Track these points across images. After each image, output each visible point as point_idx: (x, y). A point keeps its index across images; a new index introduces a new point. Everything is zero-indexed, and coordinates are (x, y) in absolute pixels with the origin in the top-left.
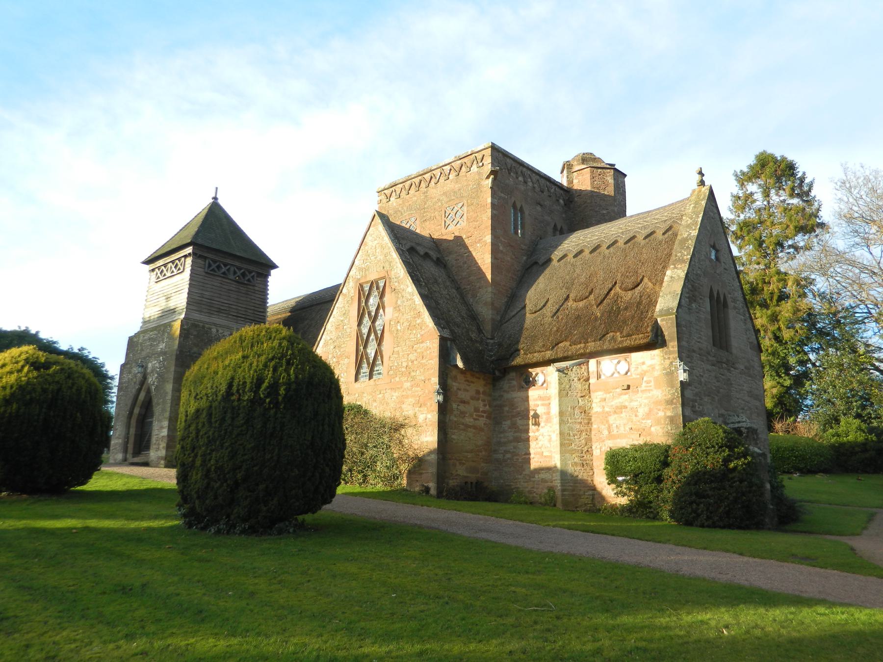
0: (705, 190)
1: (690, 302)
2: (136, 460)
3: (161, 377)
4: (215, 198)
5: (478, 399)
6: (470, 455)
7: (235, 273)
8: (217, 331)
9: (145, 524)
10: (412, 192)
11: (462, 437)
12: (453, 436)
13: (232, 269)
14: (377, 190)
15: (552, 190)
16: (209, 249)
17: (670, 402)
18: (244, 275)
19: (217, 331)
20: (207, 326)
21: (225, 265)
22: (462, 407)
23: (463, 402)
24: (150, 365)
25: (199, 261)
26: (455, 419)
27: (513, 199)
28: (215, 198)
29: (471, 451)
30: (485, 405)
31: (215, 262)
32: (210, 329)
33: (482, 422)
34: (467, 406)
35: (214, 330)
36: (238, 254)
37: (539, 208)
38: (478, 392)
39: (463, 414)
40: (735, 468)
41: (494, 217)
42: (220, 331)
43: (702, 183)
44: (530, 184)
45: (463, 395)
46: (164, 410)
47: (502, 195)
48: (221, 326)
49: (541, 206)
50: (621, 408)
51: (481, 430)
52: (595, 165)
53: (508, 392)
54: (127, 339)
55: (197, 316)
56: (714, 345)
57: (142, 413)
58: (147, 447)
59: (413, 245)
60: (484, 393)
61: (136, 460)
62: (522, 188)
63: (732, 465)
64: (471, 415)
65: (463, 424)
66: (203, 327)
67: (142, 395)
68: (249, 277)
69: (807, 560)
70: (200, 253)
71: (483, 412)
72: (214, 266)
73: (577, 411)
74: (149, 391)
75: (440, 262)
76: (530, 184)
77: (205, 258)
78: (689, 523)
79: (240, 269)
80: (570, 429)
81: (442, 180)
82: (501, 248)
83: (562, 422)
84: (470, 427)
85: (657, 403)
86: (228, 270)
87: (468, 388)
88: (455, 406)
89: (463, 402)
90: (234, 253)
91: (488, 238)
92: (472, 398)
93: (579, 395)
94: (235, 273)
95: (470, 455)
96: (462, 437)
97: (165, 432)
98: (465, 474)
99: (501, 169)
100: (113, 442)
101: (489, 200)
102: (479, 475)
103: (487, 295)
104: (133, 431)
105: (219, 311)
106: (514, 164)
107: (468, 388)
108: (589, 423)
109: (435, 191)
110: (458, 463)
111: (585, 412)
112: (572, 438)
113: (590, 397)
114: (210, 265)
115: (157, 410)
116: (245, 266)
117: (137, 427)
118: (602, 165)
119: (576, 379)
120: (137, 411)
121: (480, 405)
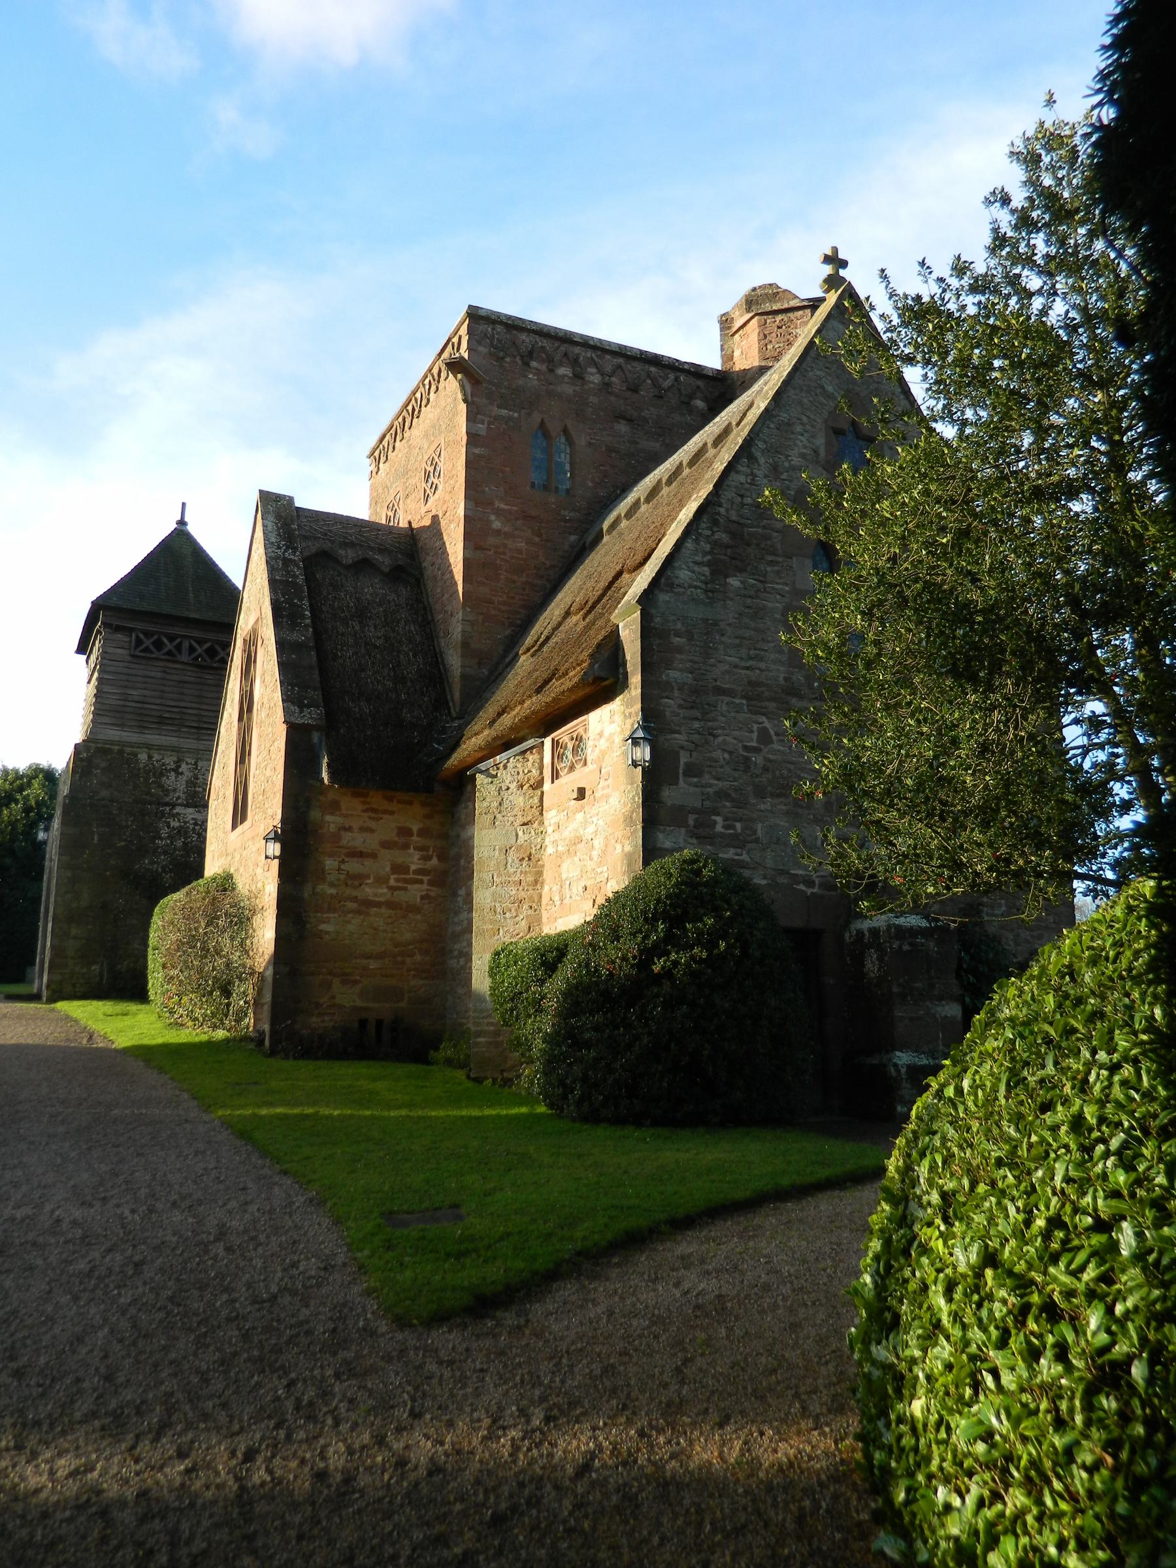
1: (719, 570)
4: (182, 522)
5: (406, 847)
6: (373, 965)
7: (192, 650)
8: (150, 757)
9: (488, 1112)
11: (350, 927)
12: (323, 927)
13: (186, 645)
14: (368, 453)
16: (135, 614)
19: (150, 757)
20: (128, 750)
21: (172, 639)
25: (119, 636)
26: (333, 891)
27: (537, 417)
28: (182, 522)
29: (380, 956)
30: (426, 858)
31: (148, 634)
32: (136, 755)
34: (368, 862)
35: (143, 757)
36: (193, 615)
37: (622, 427)
38: (405, 832)
39: (358, 879)
40: (667, 973)
42: (156, 757)
47: (504, 412)
48: (160, 748)
49: (630, 420)
51: (412, 909)
52: (768, 307)
59: (327, 546)
60: (422, 833)
63: (656, 968)
64: (381, 880)
65: (354, 899)
66: (121, 752)
70: (115, 622)
72: (148, 643)
73: (513, 856)
77: (131, 630)
78: (592, 1118)
79: (200, 642)
82: (497, 525)
84: (378, 905)
86: (179, 647)
87: (373, 825)
88: (330, 863)
90: (186, 614)
92: (386, 845)
93: (520, 820)
94: (192, 650)
95: (373, 965)
96: (350, 927)
98: (359, 1003)
103: (455, 628)
105: (161, 721)
107: (373, 825)
108: (537, 881)
110: (336, 982)
111: (530, 858)
113: (542, 823)
114: (139, 642)
116: (212, 636)
119: (513, 786)
121: (414, 861)
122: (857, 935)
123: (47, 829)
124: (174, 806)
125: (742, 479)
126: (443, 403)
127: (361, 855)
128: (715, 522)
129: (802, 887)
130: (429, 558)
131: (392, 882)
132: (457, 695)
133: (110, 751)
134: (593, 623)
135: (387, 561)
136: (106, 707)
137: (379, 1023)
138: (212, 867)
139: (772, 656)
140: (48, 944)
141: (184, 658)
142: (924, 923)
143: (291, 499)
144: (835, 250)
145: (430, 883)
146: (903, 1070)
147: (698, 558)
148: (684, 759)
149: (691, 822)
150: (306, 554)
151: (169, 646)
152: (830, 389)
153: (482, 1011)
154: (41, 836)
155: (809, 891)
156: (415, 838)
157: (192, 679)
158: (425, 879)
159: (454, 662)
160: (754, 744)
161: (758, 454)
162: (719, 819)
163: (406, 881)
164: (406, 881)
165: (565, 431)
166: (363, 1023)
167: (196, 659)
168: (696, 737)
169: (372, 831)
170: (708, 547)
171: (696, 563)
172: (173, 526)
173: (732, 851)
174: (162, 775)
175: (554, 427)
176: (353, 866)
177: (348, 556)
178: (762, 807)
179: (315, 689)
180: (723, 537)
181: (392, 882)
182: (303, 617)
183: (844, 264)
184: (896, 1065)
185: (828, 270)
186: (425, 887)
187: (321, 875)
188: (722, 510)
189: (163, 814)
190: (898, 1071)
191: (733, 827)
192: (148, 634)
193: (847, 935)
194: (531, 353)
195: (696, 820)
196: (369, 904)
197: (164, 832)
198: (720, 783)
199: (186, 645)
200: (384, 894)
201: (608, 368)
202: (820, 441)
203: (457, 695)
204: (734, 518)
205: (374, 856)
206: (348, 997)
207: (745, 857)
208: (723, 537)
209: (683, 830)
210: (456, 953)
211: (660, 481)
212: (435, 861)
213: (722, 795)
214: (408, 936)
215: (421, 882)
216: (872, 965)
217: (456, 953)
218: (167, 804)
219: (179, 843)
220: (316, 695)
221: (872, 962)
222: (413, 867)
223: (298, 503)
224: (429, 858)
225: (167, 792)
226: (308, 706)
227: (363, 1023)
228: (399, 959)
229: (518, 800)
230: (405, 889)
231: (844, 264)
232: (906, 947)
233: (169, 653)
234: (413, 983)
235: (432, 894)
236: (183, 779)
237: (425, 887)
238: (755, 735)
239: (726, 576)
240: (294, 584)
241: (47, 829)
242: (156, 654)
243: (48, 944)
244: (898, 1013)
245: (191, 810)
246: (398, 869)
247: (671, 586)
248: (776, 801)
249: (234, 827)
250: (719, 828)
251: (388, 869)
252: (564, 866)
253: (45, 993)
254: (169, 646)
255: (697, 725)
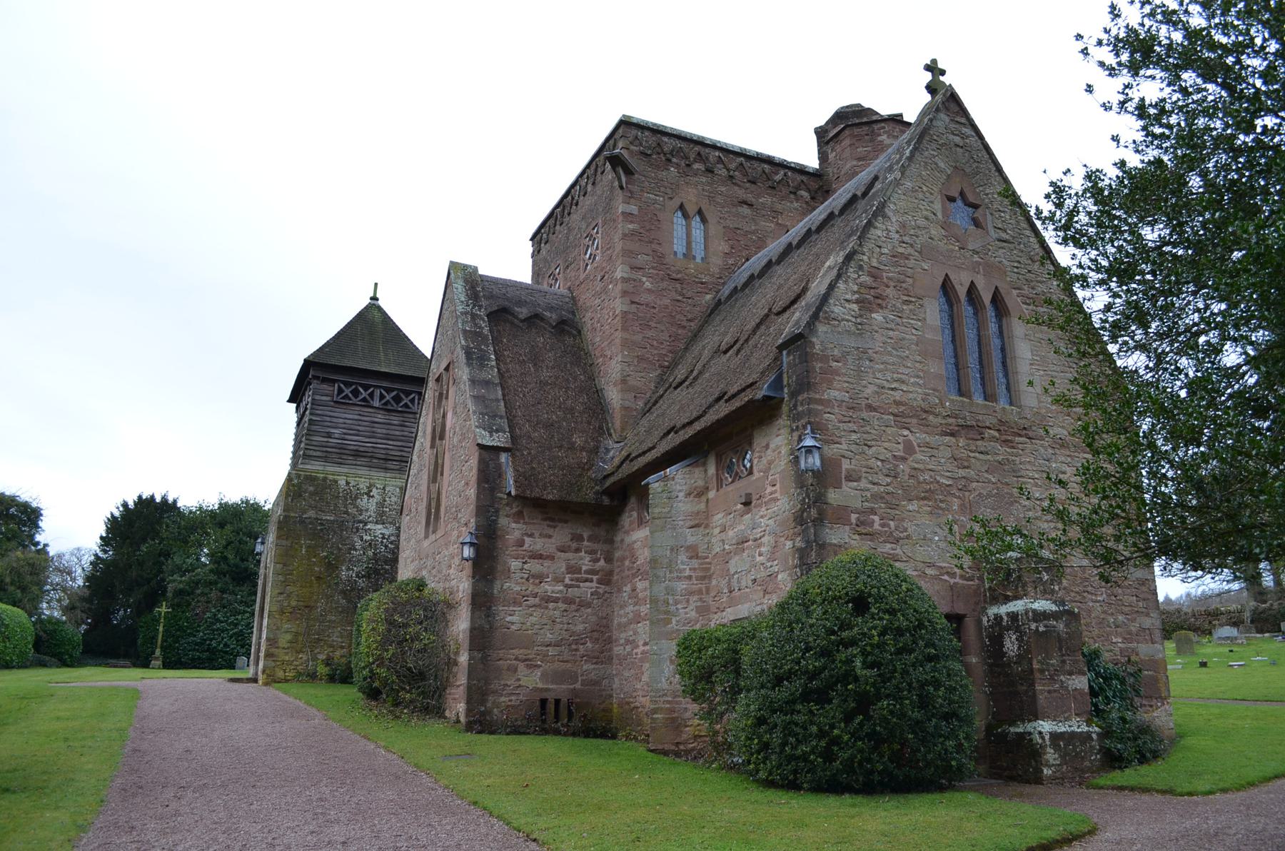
4: (374, 298)
5: (578, 550)
8: (348, 483)
13: (377, 393)
20: (331, 477)
21: (366, 388)
28: (374, 298)
35: (342, 483)
51: (583, 604)
53: (627, 532)
54: (26, 494)
64: (558, 580)
66: (325, 479)
68: (406, 401)
72: (347, 391)
75: (959, 390)
77: (334, 381)
79: (389, 390)
84: (556, 600)
86: (371, 395)
88: (515, 564)
90: (378, 369)
94: (382, 397)
98: (540, 685)
102: (578, 686)
106: (679, 144)
107: (550, 531)
110: (521, 666)
112: (673, 608)
114: (340, 391)
121: (585, 562)
122: (995, 619)
123: (263, 543)
124: (366, 524)
125: (879, 233)
126: (599, 192)
127: (541, 557)
128: (861, 268)
129: (946, 577)
130: (589, 315)
131: (567, 581)
132: (618, 424)
133: (316, 478)
134: (747, 358)
135: (554, 316)
136: (305, 446)
137: (557, 702)
138: (405, 572)
139: (912, 380)
140: (264, 636)
141: (376, 403)
142: (1054, 608)
143: (476, 269)
144: (934, 61)
145: (599, 582)
146: (1047, 737)
147: (848, 297)
148: (846, 465)
149: (854, 521)
150: (490, 310)
151: (364, 394)
152: (942, 165)
153: (658, 690)
154: (259, 548)
155: (952, 581)
156: (585, 543)
157: (318, 454)
158: (595, 578)
159: (614, 396)
160: (901, 454)
161: (890, 214)
162: (876, 518)
163: (577, 580)
164: (577, 580)
165: (700, 212)
166: (544, 702)
167: (386, 404)
168: (853, 447)
169: (550, 537)
170: (855, 288)
171: (847, 301)
172: (367, 301)
173: (889, 546)
174: (356, 498)
175: (691, 209)
176: (534, 566)
177: (523, 312)
178: (910, 508)
179: (501, 417)
180: (865, 279)
181: (567, 581)
182: (489, 359)
183: (943, 73)
184: (1040, 733)
185: (928, 76)
186: (594, 584)
187: (508, 573)
188: (865, 258)
189: (357, 529)
190: (1043, 738)
191: (888, 526)
192: (347, 384)
193: (985, 619)
194: (671, 153)
195: (858, 519)
196: (548, 600)
197: (358, 544)
198: (876, 488)
199: (377, 393)
200: (561, 591)
201: (733, 166)
202: (938, 206)
203: (618, 424)
204: (875, 264)
205: (551, 558)
206: (531, 680)
207: (899, 551)
208: (865, 279)
209: (847, 528)
210: (622, 641)
211: (790, 244)
212: (602, 562)
213: (876, 497)
214: (580, 627)
215: (591, 581)
216: (1011, 645)
217: (622, 641)
218: (360, 522)
219: (370, 553)
220: (504, 423)
221: (1012, 643)
222: (584, 568)
223: (481, 272)
224: (598, 560)
225: (361, 511)
226: (497, 431)
227: (544, 702)
228: (574, 647)
229: (684, 506)
230: (578, 587)
231: (943, 73)
232: (1041, 629)
233: (364, 400)
234: (585, 667)
235: (601, 591)
236: (373, 502)
237: (594, 584)
238: (901, 447)
239: (871, 312)
240: (479, 334)
241: (263, 543)
242: (354, 400)
243: (264, 636)
244: (1038, 688)
245: (380, 526)
246: (572, 569)
247: (828, 319)
248: (922, 502)
249: (426, 537)
250: (876, 526)
251: (563, 569)
252: (732, 562)
253: (261, 677)
254: (364, 394)
255: (854, 437)
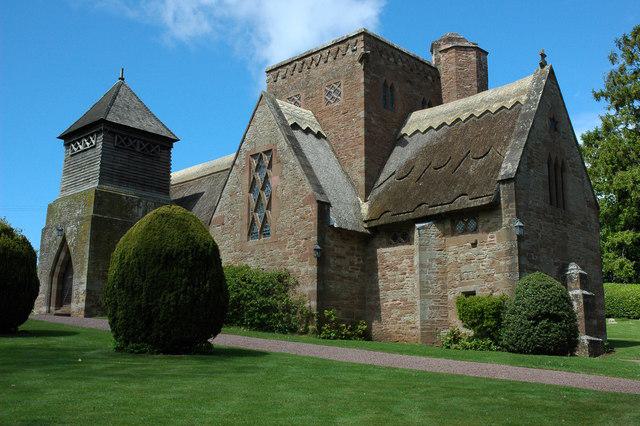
0: (547, 69)
2: (59, 312)
3: (78, 237)
6: (345, 302)
10: (296, 72)
11: (339, 287)
15: (421, 69)
17: (509, 252)
18: (149, 148)
22: (338, 262)
23: (339, 257)
24: (69, 229)
33: (357, 274)
37: (408, 85)
38: (353, 249)
41: (366, 95)
43: (542, 65)
44: (400, 64)
45: (338, 251)
46: (81, 271)
49: (410, 82)
50: (469, 260)
51: (356, 280)
52: (456, 44)
55: (107, 188)
56: (551, 204)
57: (64, 270)
58: (69, 301)
61: (59, 312)
62: (393, 68)
64: (346, 269)
67: (62, 257)
69: (382, 350)
71: (358, 265)
74: (68, 252)
76: (400, 64)
77: (115, 134)
80: (430, 278)
81: (322, 62)
82: (373, 122)
83: (421, 272)
85: (499, 255)
86: (135, 143)
88: (332, 260)
89: (339, 257)
91: (362, 114)
96: (339, 287)
97: (84, 287)
99: (372, 52)
100: (39, 296)
101: (362, 80)
104: (55, 287)
109: (315, 72)
114: (119, 140)
115: (76, 268)
117: (58, 284)
118: (466, 44)
120: (58, 270)
